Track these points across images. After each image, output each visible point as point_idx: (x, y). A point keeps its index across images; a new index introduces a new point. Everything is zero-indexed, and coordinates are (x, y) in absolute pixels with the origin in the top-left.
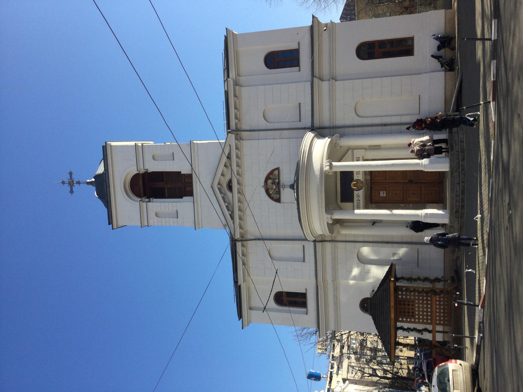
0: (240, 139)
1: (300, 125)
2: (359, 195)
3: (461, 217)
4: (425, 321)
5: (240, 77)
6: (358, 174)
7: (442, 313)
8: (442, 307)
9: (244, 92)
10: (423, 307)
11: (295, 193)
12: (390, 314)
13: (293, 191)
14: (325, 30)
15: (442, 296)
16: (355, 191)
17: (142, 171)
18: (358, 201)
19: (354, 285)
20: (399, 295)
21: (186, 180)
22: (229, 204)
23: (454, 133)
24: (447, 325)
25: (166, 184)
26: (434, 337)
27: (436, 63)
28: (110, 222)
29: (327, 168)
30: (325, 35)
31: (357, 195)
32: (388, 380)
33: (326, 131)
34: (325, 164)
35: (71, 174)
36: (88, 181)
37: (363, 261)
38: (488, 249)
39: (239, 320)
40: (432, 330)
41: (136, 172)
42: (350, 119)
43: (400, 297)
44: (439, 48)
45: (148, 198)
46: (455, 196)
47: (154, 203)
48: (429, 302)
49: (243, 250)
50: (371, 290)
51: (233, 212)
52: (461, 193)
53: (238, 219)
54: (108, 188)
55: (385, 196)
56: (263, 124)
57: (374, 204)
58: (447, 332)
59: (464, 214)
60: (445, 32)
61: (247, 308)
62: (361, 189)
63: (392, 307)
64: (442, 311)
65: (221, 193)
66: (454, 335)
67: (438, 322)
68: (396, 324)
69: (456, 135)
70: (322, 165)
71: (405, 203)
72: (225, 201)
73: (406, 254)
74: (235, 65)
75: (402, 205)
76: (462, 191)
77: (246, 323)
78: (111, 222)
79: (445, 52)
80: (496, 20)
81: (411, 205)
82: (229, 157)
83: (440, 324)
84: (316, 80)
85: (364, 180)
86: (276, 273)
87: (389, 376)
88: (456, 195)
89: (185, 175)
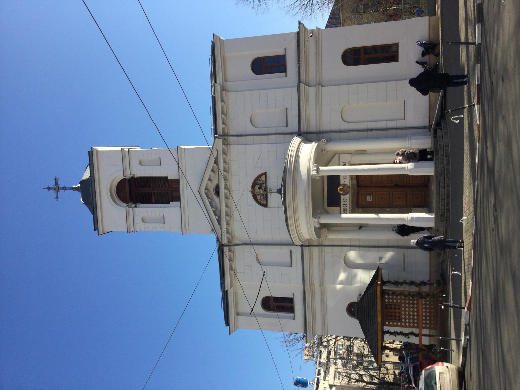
0: (228, 144)
2: (346, 199)
3: (446, 220)
4: (412, 325)
5: (227, 83)
6: (345, 179)
8: (428, 307)
9: (231, 97)
10: (409, 311)
11: (282, 197)
16: (341, 196)
17: (129, 176)
18: (344, 205)
19: (341, 290)
20: (386, 298)
21: (173, 186)
22: (216, 209)
23: (439, 137)
24: (432, 328)
26: (421, 340)
28: (96, 228)
29: (314, 173)
30: (311, 41)
32: (375, 385)
34: (312, 168)
36: (74, 186)
37: (350, 265)
38: (474, 251)
40: (418, 334)
43: (387, 300)
44: (423, 54)
45: (134, 204)
48: (415, 306)
50: (358, 294)
52: (446, 197)
55: (371, 200)
56: (250, 129)
57: (360, 208)
58: (433, 336)
59: (449, 218)
62: (347, 194)
64: (428, 314)
67: (424, 325)
68: (382, 328)
69: (441, 139)
71: (390, 207)
73: (392, 258)
75: (388, 209)
78: (96, 228)
81: (397, 210)
82: (216, 162)
83: (426, 328)
84: (302, 86)
86: (264, 274)
87: (376, 381)
88: (441, 199)
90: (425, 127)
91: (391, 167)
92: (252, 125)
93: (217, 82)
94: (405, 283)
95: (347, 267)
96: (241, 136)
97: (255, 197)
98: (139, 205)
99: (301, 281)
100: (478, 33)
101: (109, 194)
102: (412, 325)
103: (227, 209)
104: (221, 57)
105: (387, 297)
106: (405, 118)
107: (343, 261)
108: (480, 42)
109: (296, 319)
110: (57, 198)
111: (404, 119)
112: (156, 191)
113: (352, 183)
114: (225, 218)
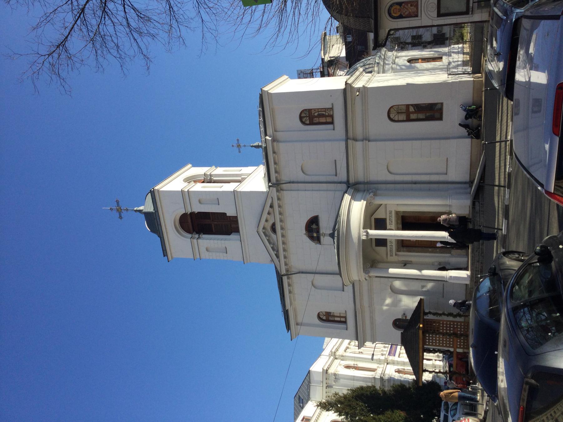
0: (281, 190)
1: (335, 179)
4: (448, 323)
5: (277, 133)
7: (463, 328)
9: (282, 148)
14: (358, 95)
15: (462, 338)
17: (189, 211)
19: (387, 310)
20: (427, 337)
22: (274, 244)
23: (477, 212)
25: (213, 221)
27: (464, 131)
28: (165, 254)
29: (364, 238)
30: (358, 102)
31: (390, 241)
33: (361, 186)
34: (362, 233)
35: (118, 202)
36: (135, 209)
37: (395, 291)
39: (288, 332)
40: (453, 352)
44: (466, 118)
46: (475, 271)
47: (205, 241)
48: (451, 343)
50: (403, 313)
51: (278, 251)
56: (301, 176)
61: (293, 315)
63: (417, 32)
65: (266, 235)
66: (487, 143)
72: (270, 243)
73: (433, 288)
75: (430, 250)
76: (481, 270)
77: (294, 336)
78: (165, 254)
79: (473, 122)
81: (438, 250)
82: (271, 206)
83: (460, 348)
84: (350, 142)
88: (476, 271)
90: (465, 183)
91: (433, 236)
92: (302, 173)
93: (268, 133)
94: (444, 314)
95: (393, 293)
96: (293, 182)
98: (202, 235)
100: (504, 228)
102: (448, 345)
105: (427, 335)
106: (448, 171)
107: (390, 288)
108: (506, 234)
109: (348, 329)
110: (121, 218)
111: (446, 174)
112: (216, 223)
113: (397, 227)
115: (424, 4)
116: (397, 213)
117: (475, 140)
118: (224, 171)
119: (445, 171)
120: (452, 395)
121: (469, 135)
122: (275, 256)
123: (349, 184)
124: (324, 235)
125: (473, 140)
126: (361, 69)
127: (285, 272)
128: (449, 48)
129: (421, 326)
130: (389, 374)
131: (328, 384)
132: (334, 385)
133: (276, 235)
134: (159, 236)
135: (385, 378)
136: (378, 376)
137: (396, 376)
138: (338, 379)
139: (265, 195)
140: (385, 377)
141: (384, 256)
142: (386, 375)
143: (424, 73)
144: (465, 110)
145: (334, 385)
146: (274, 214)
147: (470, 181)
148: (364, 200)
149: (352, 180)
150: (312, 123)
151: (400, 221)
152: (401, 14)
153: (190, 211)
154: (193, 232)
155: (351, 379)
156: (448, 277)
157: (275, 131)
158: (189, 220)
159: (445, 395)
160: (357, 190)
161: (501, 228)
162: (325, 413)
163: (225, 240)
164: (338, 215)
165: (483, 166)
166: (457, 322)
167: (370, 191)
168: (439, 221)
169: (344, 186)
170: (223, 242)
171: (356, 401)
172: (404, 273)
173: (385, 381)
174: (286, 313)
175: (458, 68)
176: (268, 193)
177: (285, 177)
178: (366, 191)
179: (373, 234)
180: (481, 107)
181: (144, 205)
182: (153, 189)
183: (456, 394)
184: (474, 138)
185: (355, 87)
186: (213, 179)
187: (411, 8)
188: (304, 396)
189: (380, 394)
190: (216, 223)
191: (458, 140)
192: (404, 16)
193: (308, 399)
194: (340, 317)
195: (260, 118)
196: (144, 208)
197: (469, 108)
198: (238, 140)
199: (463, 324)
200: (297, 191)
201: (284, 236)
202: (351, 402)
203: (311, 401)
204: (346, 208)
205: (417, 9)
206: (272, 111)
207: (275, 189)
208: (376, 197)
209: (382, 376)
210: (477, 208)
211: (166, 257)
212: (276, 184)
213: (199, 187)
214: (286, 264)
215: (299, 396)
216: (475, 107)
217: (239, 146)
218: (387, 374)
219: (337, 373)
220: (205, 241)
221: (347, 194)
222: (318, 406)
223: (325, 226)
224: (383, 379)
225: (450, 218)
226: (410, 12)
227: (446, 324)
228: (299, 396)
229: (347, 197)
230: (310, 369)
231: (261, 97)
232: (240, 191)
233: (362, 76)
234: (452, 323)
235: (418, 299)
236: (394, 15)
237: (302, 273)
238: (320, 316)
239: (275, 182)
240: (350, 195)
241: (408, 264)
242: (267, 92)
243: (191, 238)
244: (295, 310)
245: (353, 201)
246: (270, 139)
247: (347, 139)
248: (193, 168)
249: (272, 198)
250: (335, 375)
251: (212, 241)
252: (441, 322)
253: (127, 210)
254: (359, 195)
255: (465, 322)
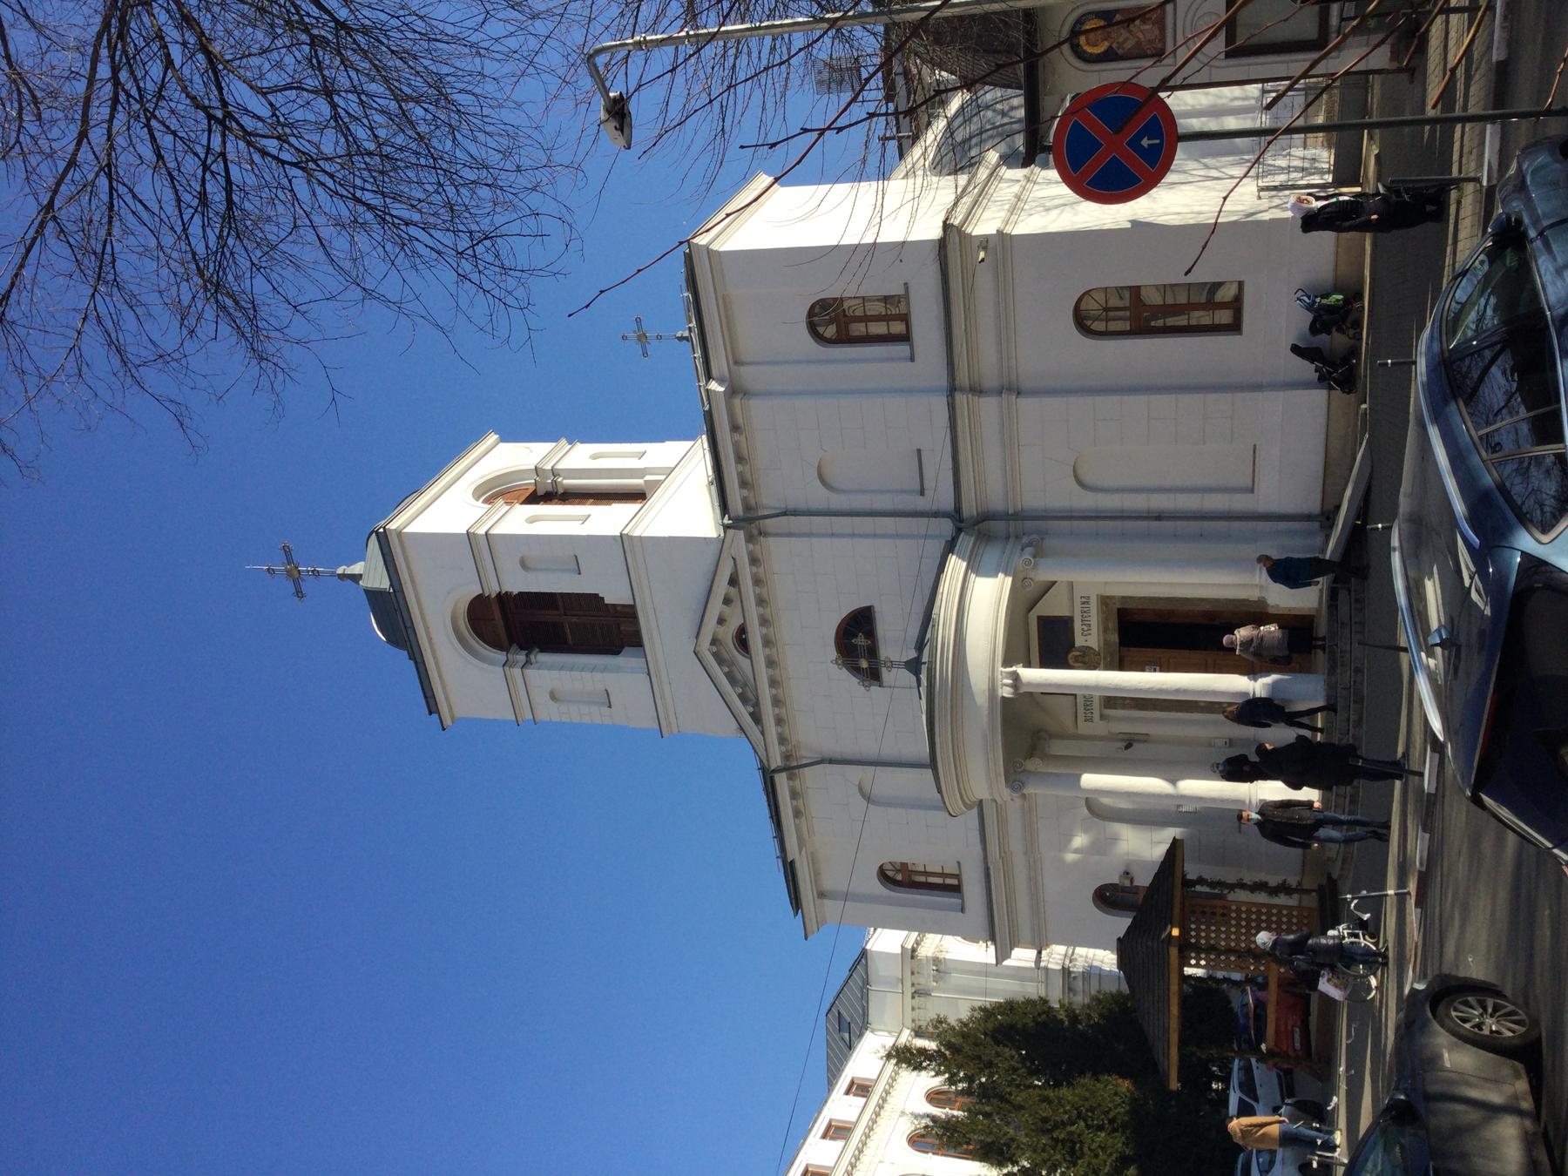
1: (922, 504)
4: (1254, 909)
5: (742, 368)
9: (757, 412)
11: (919, 685)
12: (1169, 1006)
13: (913, 678)
14: (983, 260)
17: (493, 589)
19: (1075, 864)
20: (1192, 930)
22: (745, 685)
27: (1307, 369)
28: (432, 707)
29: (1007, 692)
30: (984, 282)
33: (997, 526)
34: (1000, 677)
36: (340, 571)
41: (477, 591)
42: (1059, 494)
44: (1314, 329)
49: (762, 615)
51: (757, 704)
53: (760, 645)
54: (410, 631)
56: (819, 496)
60: (1336, 277)
70: (993, 679)
74: (721, 322)
77: (812, 925)
78: (433, 709)
79: (1336, 341)
80: (1427, 836)
82: (734, 581)
84: (961, 398)
85: (1102, 645)
89: (619, 608)
90: (1308, 517)
96: (795, 513)
97: (813, 307)
99: (977, 840)
101: (455, 641)
103: (745, 492)
104: (717, 300)
108: (1433, 791)
111: (1252, 491)
112: (574, 619)
113: (1105, 640)
114: (738, 493)
115: (1185, 21)
116: (1105, 601)
117: (1337, 393)
118: (595, 457)
119: (1248, 482)
120: (1261, 1132)
121: (1321, 379)
122: (749, 720)
123: (961, 520)
124: (889, 664)
125: (1333, 392)
126: (993, 156)
127: (780, 764)
128: (1261, 170)
129: (1175, 932)
130: (1086, 957)
131: (917, 987)
132: (934, 989)
133: (751, 658)
134: (412, 657)
135: (1075, 970)
136: (1057, 964)
137: (1106, 960)
138: (945, 973)
139: (715, 548)
140: (1075, 966)
141: (1068, 721)
142: (1079, 959)
143: (1185, 172)
144: (1309, 308)
145: (934, 989)
146: (742, 602)
147: (1322, 513)
148: (1006, 574)
149: (969, 509)
150: (844, 339)
151: (1113, 624)
152: (1111, 46)
153: (498, 590)
154: (511, 645)
155: (979, 973)
156: (1254, 802)
157: (736, 363)
158: (497, 614)
159: (1241, 1130)
160: (985, 538)
161: (1416, 768)
162: (907, 1076)
163: (605, 669)
164: (927, 619)
165: (1363, 486)
166: (1280, 908)
167: (1025, 540)
168: (1238, 1139)
169: (947, 527)
170: (597, 676)
171: (995, 1047)
172: (1126, 790)
173: (1075, 978)
174: (790, 871)
175: (1289, 154)
176: (722, 542)
177: (771, 495)
178: (1012, 540)
179: (1034, 682)
180: (1359, 296)
181: (363, 559)
182: (384, 528)
183: (1274, 1130)
184: (1335, 389)
185: (973, 234)
186: (561, 482)
187: (1142, 27)
188: (852, 1017)
189: (1062, 1022)
190: (574, 619)
191: (1289, 393)
192: (1120, 52)
193: (864, 1026)
194: (942, 875)
195: (690, 322)
196: (365, 567)
197: (1324, 301)
198: (638, 321)
199: (1295, 913)
200: (806, 539)
201: (778, 682)
202: (982, 1048)
203: (872, 1032)
204: (953, 602)
205: (1163, 29)
206: (725, 304)
207: (741, 534)
208: (1042, 560)
209: (1067, 962)
210: (1344, 610)
211: (435, 716)
212: (744, 520)
213: (519, 521)
214: (782, 740)
215: (839, 1013)
216: (1341, 297)
217: (642, 338)
218: (1081, 956)
219: (941, 956)
220: (546, 672)
221: (954, 557)
222: (889, 1056)
223: (893, 640)
224: (1070, 973)
225: (1262, 638)
226: (1139, 43)
227: (1249, 912)
228: (839, 1013)
229: (956, 566)
230: (868, 947)
231: (689, 259)
232: (640, 538)
233: (996, 183)
234: (1264, 910)
235: (1170, 833)
236: (1089, 49)
237: (831, 761)
238: (887, 872)
239: (741, 512)
240: (964, 560)
241: (1139, 741)
242: (707, 248)
243: (504, 665)
244: (813, 860)
245: (973, 576)
246: (722, 389)
247: (952, 390)
248: (501, 444)
249: (734, 559)
250: (936, 961)
251: (565, 674)
252: (1234, 908)
253: (316, 574)
254: (991, 554)
255: (1299, 907)
